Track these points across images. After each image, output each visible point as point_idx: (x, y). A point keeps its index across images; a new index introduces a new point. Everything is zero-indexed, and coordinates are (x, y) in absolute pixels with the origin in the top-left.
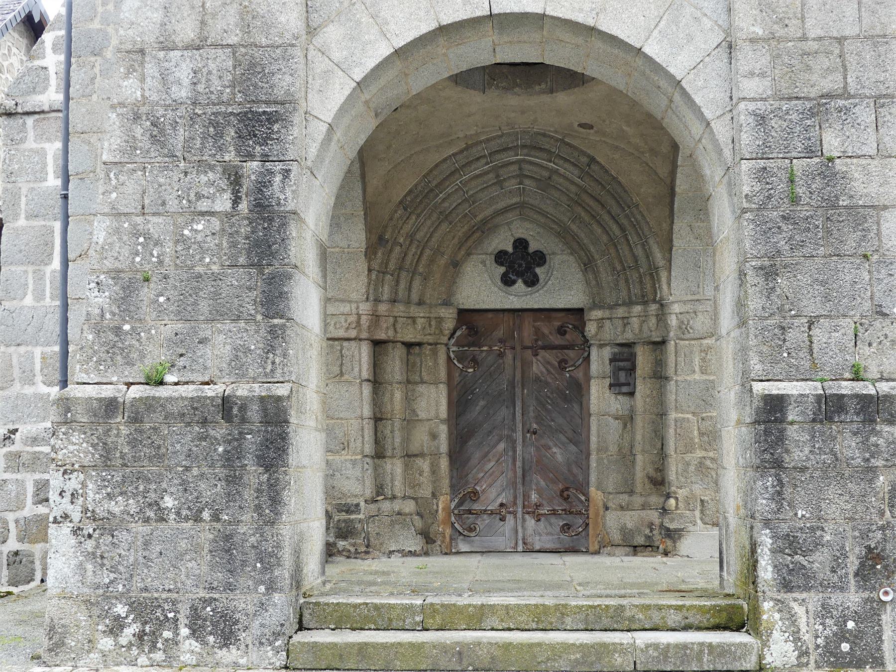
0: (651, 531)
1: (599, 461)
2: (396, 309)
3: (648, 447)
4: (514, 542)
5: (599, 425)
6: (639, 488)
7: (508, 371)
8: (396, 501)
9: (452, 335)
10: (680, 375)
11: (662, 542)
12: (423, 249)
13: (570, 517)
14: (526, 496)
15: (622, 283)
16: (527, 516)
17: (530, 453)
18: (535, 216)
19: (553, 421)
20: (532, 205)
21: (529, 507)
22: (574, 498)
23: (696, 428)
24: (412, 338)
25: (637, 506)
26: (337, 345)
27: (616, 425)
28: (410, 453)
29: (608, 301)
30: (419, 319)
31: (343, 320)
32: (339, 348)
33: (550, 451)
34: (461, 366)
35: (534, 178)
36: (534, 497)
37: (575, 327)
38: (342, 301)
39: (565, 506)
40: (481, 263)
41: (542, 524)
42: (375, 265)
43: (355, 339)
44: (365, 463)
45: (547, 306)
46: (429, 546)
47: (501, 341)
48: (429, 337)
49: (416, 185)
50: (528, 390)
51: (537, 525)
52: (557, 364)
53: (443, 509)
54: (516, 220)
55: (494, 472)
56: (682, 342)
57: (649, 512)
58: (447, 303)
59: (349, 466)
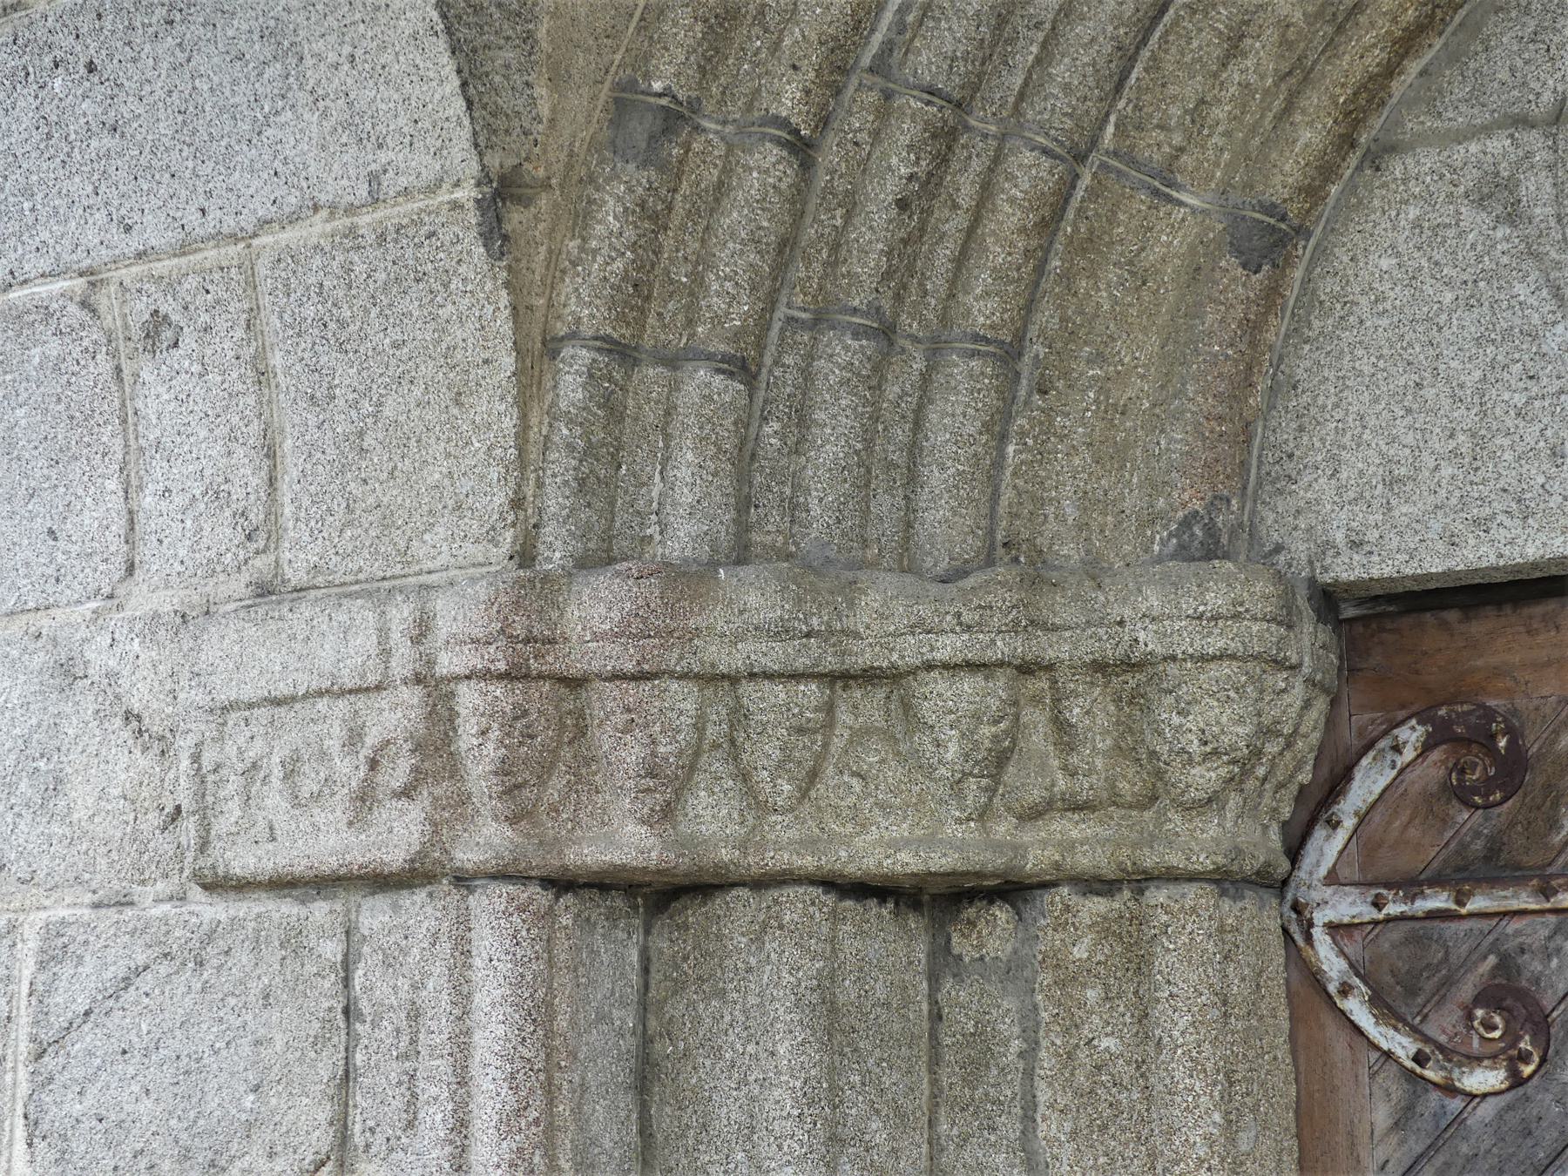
2: (717, 618)
12: (997, 160)
24: (896, 845)
26: (322, 933)
30: (938, 684)
32: (332, 950)
40: (1481, 202)
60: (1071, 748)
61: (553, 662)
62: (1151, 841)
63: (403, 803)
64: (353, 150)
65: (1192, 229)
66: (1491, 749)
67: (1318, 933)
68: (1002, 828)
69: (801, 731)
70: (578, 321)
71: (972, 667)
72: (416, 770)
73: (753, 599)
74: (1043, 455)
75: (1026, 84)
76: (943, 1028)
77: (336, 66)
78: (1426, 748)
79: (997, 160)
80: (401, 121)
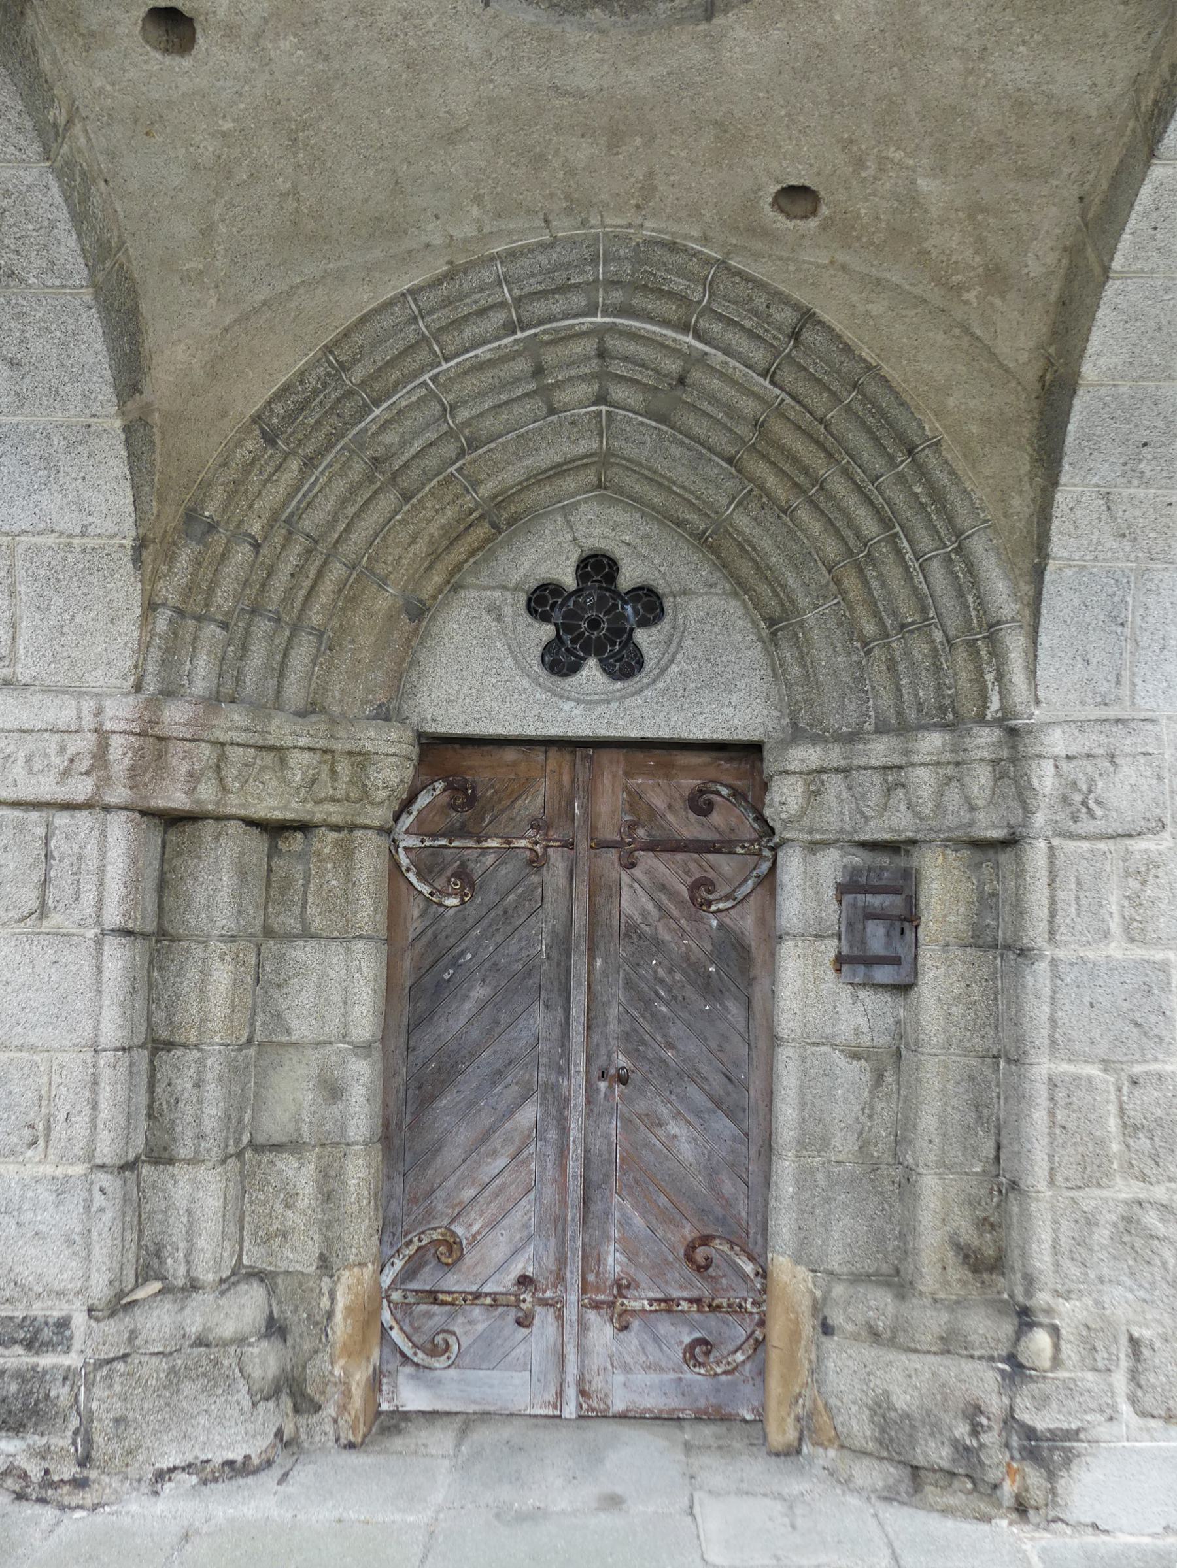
0: (975, 1433)
1: (805, 1176)
2: (221, 722)
3: (955, 1154)
4: (553, 1389)
5: (805, 1072)
6: (929, 1281)
7: (554, 908)
8: (197, 1297)
9: (405, 806)
10: (1066, 944)
11: (1010, 1471)
12: (325, 563)
13: (713, 1320)
14: (591, 1258)
15: (878, 671)
16: (592, 1315)
17: (607, 1136)
18: (638, 488)
19: (671, 1046)
20: (629, 460)
21: (598, 1290)
22: (723, 1265)
23: (1113, 1108)
24: (274, 809)
25: (926, 1339)
26: (35, 824)
27: (853, 1073)
28: (261, 1139)
29: (834, 722)
30: (297, 754)
31: (52, 749)
32: (41, 831)
33: (660, 1132)
34: (426, 889)
35: (638, 382)
36: (614, 1262)
37: (736, 793)
38: (61, 691)
39: (700, 1288)
40: (489, 612)
41: (632, 1339)
42: (169, 592)
43: (87, 805)
44: (96, 1188)
45: (665, 733)
46: (302, 1421)
47: (536, 825)
48: (330, 807)
49: (302, 375)
50: (605, 961)
51: (621, 1342)
52: (684, 892)
53: (349, 1310)
54: (586, 501)
55: (504, 1186)
56: (1070, 846)
57: (968, 1366)
58: (385, 715)
59: (46, 1195)
60: (336, 780)
61: (157, 731)
62: (359, 814)
63: (85, 777)
64: (76, 513)
65: (390, 601)
66: (466, 793)
67: (400, 850)
68: (309, 806)
69: (246, 765)
70: (167, 599)
71: (310, 749)
72: (92, 765)
73: (236, 717)
74: (328, 672)
75: (339, 537)
76: (272, 875)
77: (75, 479)
78: (444, 790)
79: (325, 563)
80: (102, 508)
